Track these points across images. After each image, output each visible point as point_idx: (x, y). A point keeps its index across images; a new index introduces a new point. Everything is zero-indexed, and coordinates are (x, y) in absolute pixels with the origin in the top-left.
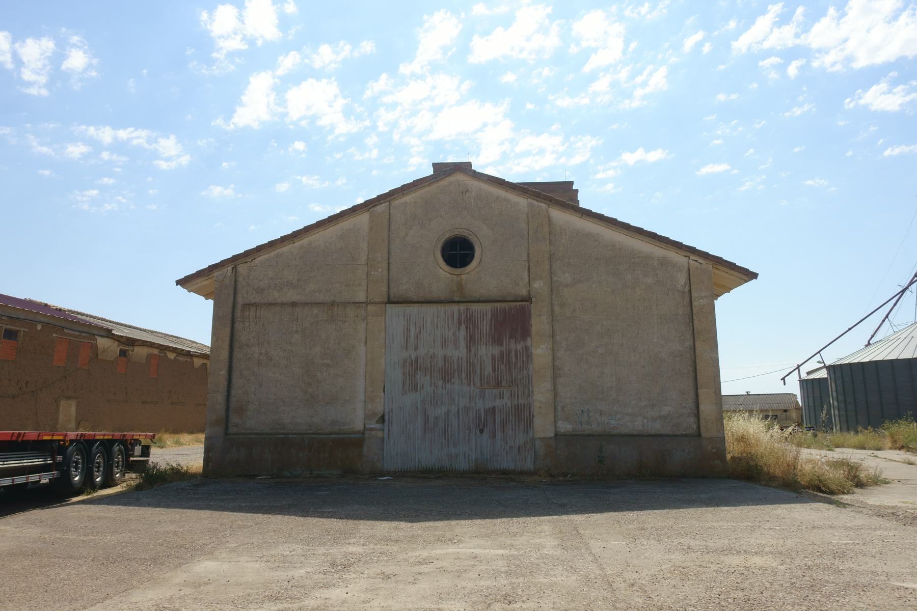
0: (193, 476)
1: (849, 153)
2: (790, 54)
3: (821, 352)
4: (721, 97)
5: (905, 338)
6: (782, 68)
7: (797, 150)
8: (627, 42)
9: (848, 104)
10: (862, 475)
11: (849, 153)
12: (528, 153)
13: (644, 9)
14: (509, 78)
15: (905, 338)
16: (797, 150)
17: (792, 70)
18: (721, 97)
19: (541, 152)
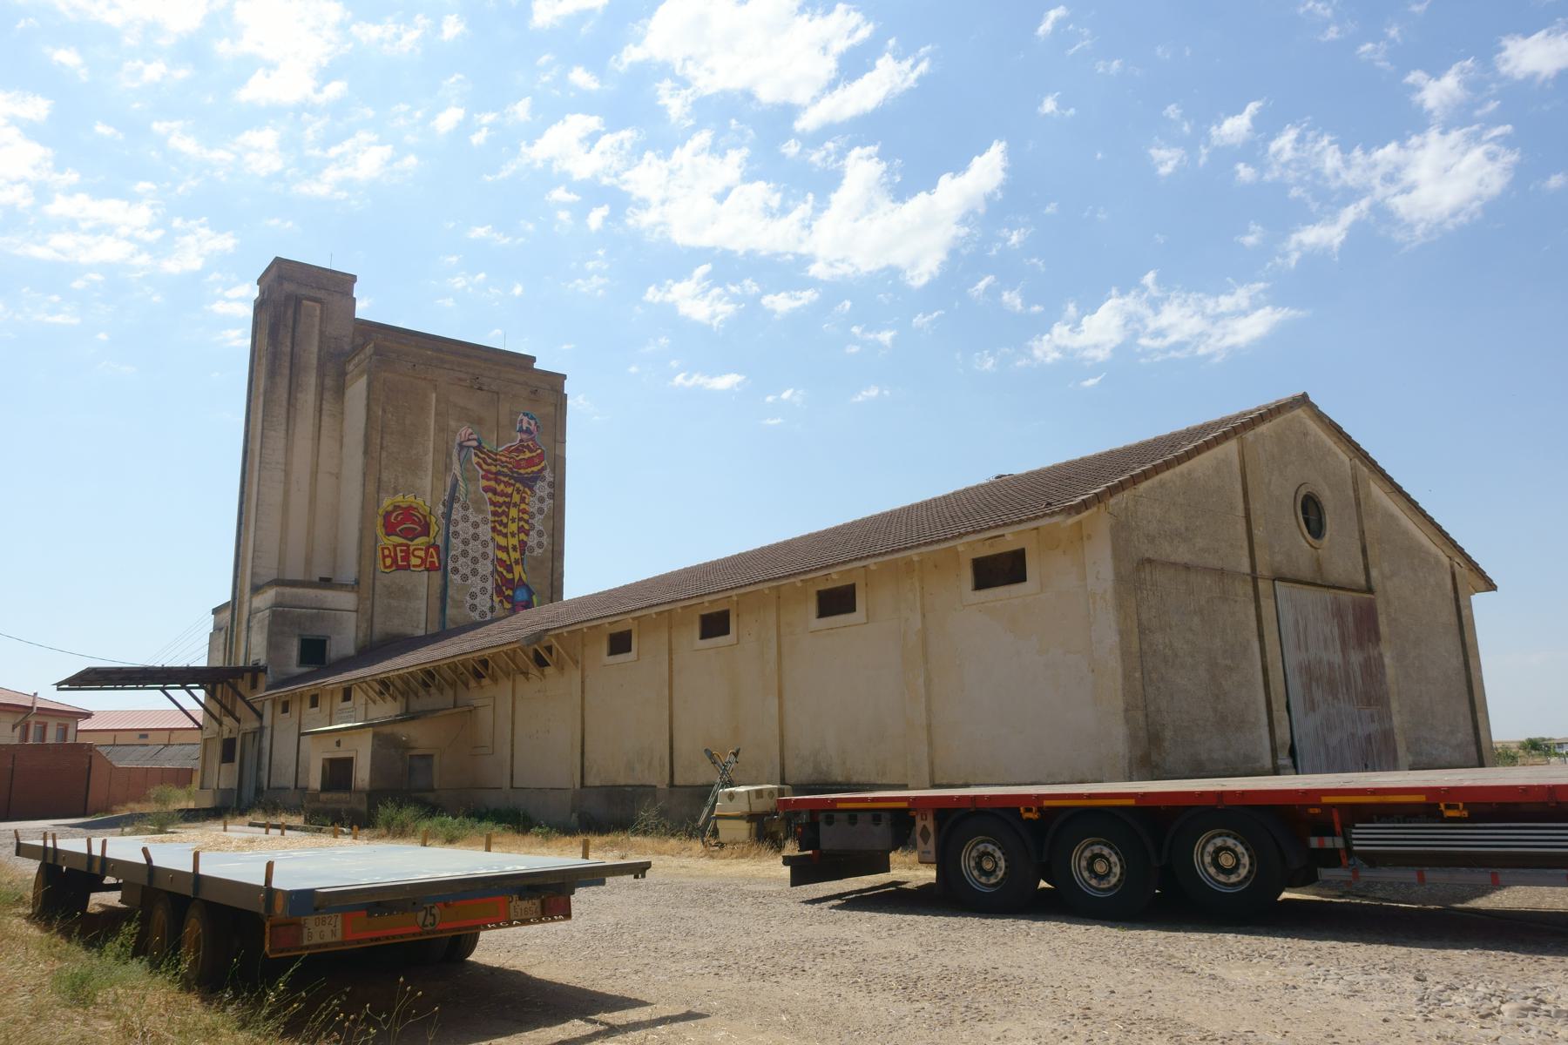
0: (353, 657)
1: (633, 369)
2: (594, 193)
3: (112, 743)
4: (480, 232)
5: (1364, 551)
6: (581, 212)
7: (565, 347)
8: (326, 75)
9: (652, 294)
10: (365, 913)
11: (633, 369)
12: (72, 225)
13: (1320, 6)
14: (66, 57)
15: (1364, 551)
16: (565, 347)
17: (596, 218)
18: (480, 232)
19: (103, 229)
